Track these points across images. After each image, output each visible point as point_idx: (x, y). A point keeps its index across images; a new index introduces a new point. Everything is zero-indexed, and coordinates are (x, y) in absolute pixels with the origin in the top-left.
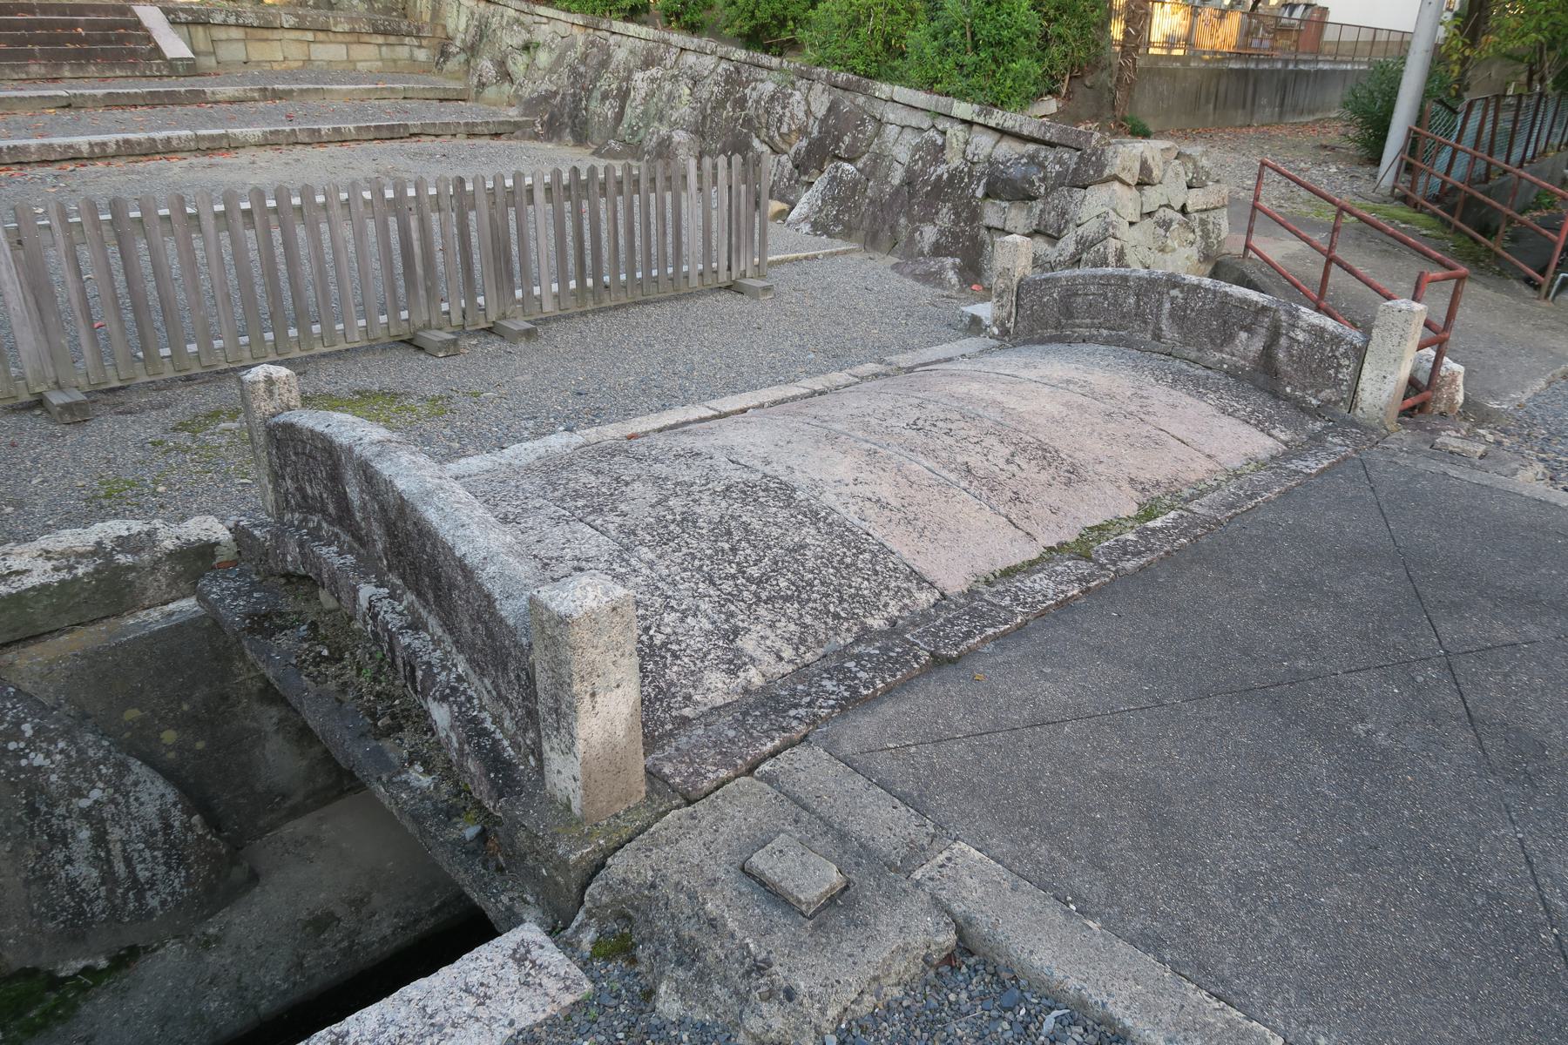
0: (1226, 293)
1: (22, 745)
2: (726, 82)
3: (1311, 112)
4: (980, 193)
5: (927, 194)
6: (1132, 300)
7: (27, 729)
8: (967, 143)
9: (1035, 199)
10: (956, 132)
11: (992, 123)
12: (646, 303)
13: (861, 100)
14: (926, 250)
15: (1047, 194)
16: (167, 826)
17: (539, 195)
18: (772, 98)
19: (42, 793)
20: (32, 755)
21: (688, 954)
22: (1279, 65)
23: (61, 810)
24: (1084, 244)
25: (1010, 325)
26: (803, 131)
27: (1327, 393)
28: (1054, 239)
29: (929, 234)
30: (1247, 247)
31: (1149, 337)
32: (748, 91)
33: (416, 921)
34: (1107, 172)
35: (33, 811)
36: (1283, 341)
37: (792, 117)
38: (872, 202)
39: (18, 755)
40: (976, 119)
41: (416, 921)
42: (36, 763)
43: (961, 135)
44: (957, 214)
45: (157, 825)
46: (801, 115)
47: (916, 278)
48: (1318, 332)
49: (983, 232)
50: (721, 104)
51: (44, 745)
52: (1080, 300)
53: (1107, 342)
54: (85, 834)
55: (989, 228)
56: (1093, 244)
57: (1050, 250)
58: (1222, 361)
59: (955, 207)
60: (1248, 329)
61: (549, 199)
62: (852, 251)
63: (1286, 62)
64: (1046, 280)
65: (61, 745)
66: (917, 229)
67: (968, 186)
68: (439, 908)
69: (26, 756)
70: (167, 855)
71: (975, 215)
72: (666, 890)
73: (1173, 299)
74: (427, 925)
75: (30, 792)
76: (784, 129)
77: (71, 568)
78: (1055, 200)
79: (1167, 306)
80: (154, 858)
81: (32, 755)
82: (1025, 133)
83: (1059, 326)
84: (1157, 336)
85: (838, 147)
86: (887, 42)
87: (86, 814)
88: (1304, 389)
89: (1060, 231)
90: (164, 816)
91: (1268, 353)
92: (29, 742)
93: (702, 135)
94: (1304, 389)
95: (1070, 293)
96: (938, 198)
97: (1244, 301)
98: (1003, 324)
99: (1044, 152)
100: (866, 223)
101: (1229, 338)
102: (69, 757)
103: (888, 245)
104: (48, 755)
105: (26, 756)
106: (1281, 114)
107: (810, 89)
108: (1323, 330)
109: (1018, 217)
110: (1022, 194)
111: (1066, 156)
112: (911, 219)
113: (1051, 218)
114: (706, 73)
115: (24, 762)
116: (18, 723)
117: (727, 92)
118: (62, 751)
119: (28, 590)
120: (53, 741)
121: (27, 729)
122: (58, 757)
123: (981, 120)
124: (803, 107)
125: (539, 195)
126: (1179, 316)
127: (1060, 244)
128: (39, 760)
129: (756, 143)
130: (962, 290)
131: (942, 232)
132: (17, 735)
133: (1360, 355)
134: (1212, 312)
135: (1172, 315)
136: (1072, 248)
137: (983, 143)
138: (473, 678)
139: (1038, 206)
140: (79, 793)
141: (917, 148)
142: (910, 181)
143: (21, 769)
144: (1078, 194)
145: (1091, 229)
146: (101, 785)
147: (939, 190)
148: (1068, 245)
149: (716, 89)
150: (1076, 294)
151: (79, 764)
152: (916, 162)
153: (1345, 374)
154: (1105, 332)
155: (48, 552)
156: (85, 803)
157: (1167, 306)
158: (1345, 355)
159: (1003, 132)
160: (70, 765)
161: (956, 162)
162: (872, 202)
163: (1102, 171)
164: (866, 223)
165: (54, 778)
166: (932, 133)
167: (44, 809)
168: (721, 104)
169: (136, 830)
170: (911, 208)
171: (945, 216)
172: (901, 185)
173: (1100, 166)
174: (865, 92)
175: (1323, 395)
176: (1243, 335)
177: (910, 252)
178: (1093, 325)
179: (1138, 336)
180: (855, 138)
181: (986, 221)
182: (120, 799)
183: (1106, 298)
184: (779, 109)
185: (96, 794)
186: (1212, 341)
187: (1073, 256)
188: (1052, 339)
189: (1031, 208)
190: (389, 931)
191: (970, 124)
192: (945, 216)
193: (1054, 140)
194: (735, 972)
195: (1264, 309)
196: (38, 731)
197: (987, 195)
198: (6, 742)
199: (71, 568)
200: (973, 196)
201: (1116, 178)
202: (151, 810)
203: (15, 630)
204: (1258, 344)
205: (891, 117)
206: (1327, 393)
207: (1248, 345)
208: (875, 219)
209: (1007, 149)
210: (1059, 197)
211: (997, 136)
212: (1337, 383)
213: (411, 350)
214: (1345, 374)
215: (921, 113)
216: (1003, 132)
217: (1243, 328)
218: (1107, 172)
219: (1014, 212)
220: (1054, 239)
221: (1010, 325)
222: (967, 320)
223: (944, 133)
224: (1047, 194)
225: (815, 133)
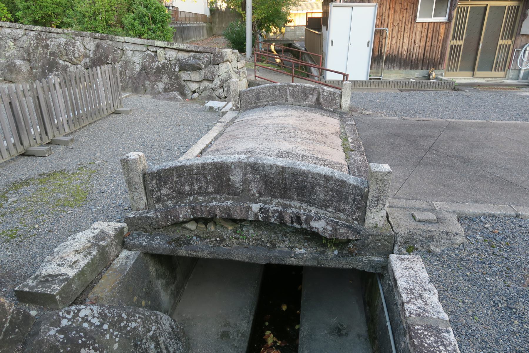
0: (305, 86)
1: (125, 322)
2: (36, 39)
3: (189, 39)
4: (177, 70)
5: (155, 72)
6: (278, 92)
7: (124, 315)
8: (165, 54)
9: (201, 69)
10: (160, 51)
11: (175, 47)
12: (94, 122)
13: (110, 43)
14: (161, 91)
15: (205, 68)
16: (173, 329)
17: (57, 86)
18: (66, 44)
19: (138, 337)
20: (130, 324)
21: (431, 239)
22: (179, 25)
23: (144, 341)
24: (223, 81)
25: (239, 106)
26: (85, 56)
27: (334, 107)
28: (211, 81)
29: (160, 86)
30: (255, 77)
31: (284, 101)
32: (48, 42)
33: (249, 318)
34: (225, 59)
35: (136, 345)
36: (321, 96)
37: (79, 50)
38: (130, 78)
39: (126, 327)
40: (167, 46)
41: (249, 318)
42: (133, 327)
43: (162, 52)
44: (170, 78)
45: (171, 330)
46: (82, 50)
47: (167, 100)
48: (330, 92)
49: (183, 82)
50: (36, 48)
51: (132, 318)
52: (261, 94)
53: (273, 105)
54: (152, 346)
55: (184, 81)
56: (226, 81)
57: (210, 85)
58: (306, 104)
59: (168, 75)
60: (312, 94)
61: (61, 87)
62: (129, 96)
63: (180, 24)
64: (250, 90)
65: (137, 315)
66: (155, 84)
67: (171, 67)
68: (250, 312)
69: (128, 326)
70: (176, 340)
71: (177, 77)
72: (413, 231)
73: (290, 90)
74: (252, 317)
75: (135, 339)
76: (77, 55)
77: (90, 254)
78: (208, 69)
79: (288, 92)
80: (173, 342)
81: (130, 324)
82: (189, 49)
83: (255, 103)
84: (287, 101)
85: (108, 60)
86: (107, 22)
87: (152, 338)
88: (328, 107)
89: (213, 78)
90: (171, 326)
91: (318, 99)
92: (127, 320)
93: (30, 61)
94: (328, 107)
95: (258, 93)
96: (160, 73)
97: (310, 87)
98: (236, 106)
99: (198, 55)
100: (130, 85)
101: (307, 98)
102: (142, 318)
103: (143, 91)
104: (136, 321)
105: (128, 326)
106: (183, 40)
107: (83, 40)
108: (331, 91)
109: (195, 76)
110: (196, 68)
111: (208, 55)
112: (151, 81)
113: (209, 75)
114: (20, 36)
115: (129, 329)
116: (120, 315)
117: (38, 43)
118: (139, 318)
119: (84, 267)
120: (134, 316)
121: (124, 315)
122: (139, 320)
123: (169, 46)
124: (82, 47)
125: (57, 86)
126: (293, 94)
127: (214, 82)
128: (133, 325)
129: (61, 62)
130: (184, 101)
131: (166, 84)
132: (122, 320)
133: (341, 96)
134: (301, 92)
135: (290, 94)
136: (219, 83)
137: (173, 54)
138: (320, 211)
139: (202, 72)
140: (149, 330)
141: (144, 58)
142: (144, 69)
143: (129, 332)
144: (217, 66)
145: (224, 76)
146: (154, 324)
147: (159, 71)
148: (217, 81)
149: (32, 42)
150: (260, 93)
151: (145, 320)
152: (145, 62)
153: (338, 101)
154: (271, 102)
155: (77, 251)
156: (151, 334)
157: (288, 92)
158: (337, 96)
159: (179, 50)
160: (144, 321)
161: (163, 61)
162: (130, 78)
163: (223, 59)
164: (130, 85)
165: (140, 329)
166: (148, 52)
167: (139, 343)
168: (36, 48)
169: (167, 335)
170: (149, 78)
171: (165, 78)
172: (141, 70)
173: (222, 58)
174: (111, 40)
175: (333, 107)
176: (311, 96)
177: (156, 94)
178: (267, 101)
179: (281, 102)
180: (114, 56)
181: (183, 79)
182: (160, 326)
183: (270, 93)
184: (71, 48)
185: (154, 328)
186: (302, 99)
187: (220, 85)
188: (255, 107)
189: (200, 73)
190: (246, 325)
191: (164, 48)
192: (165, 78)
193: (201, 51)
194: (445, 236)
195: (315, 89)
196: (128, 314)
197: (180, 70)
198: (120, 324)
199: (90, 254)
200: (175, 71)
201: (228, 60)
202: (168, 325)
203: (83, 286)
204: (315, 98)
205: (127, 48)
206: (334, 107)
207: (312, 98)
208: (134, 83)
209: (181, 55)
210: (210, 68)
211: (177, 51)
212: (336, 104)
213: (26, 157)
214: (338, 101)
215: (140, 46)
216: (179, 50)
217: (310, 94)
218: (225, 59)
219: (193, 75)
220: (211, 81)
221: (239, 106)
222: (208, 108)
223: (156, 52)
224: (205, 68)
225: (92, 56)
